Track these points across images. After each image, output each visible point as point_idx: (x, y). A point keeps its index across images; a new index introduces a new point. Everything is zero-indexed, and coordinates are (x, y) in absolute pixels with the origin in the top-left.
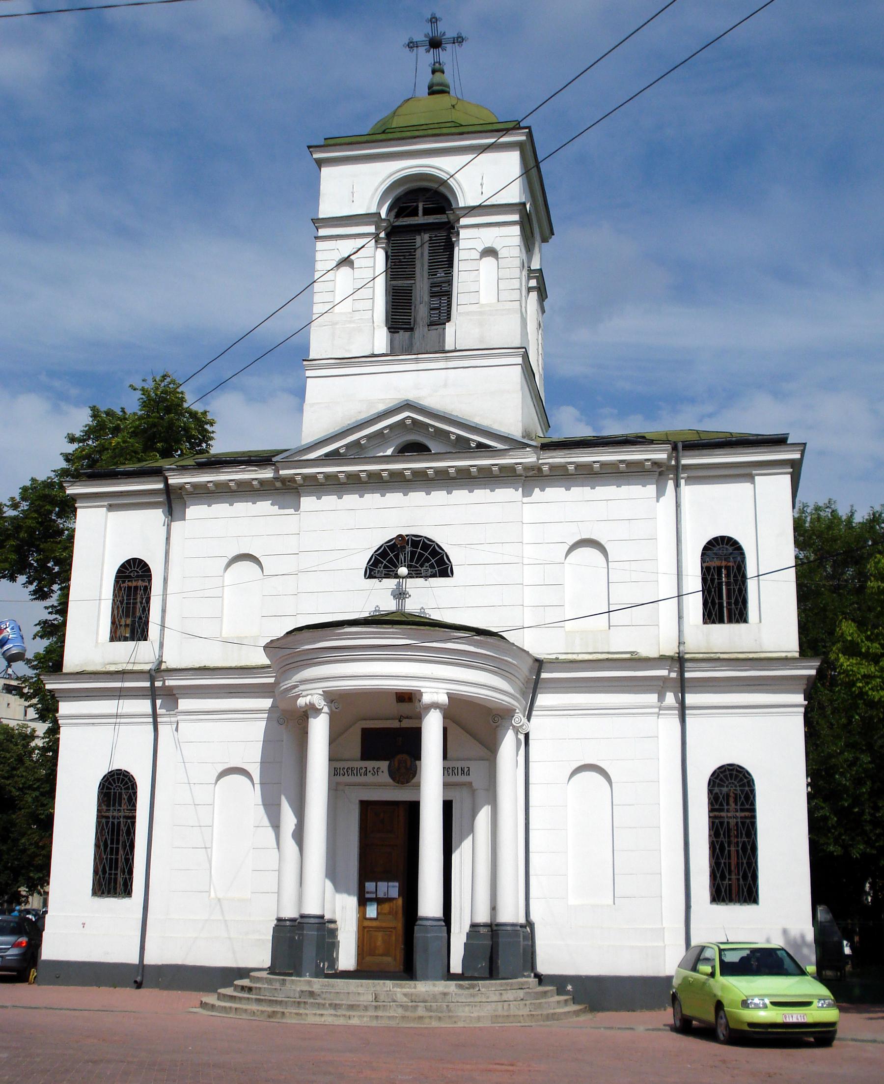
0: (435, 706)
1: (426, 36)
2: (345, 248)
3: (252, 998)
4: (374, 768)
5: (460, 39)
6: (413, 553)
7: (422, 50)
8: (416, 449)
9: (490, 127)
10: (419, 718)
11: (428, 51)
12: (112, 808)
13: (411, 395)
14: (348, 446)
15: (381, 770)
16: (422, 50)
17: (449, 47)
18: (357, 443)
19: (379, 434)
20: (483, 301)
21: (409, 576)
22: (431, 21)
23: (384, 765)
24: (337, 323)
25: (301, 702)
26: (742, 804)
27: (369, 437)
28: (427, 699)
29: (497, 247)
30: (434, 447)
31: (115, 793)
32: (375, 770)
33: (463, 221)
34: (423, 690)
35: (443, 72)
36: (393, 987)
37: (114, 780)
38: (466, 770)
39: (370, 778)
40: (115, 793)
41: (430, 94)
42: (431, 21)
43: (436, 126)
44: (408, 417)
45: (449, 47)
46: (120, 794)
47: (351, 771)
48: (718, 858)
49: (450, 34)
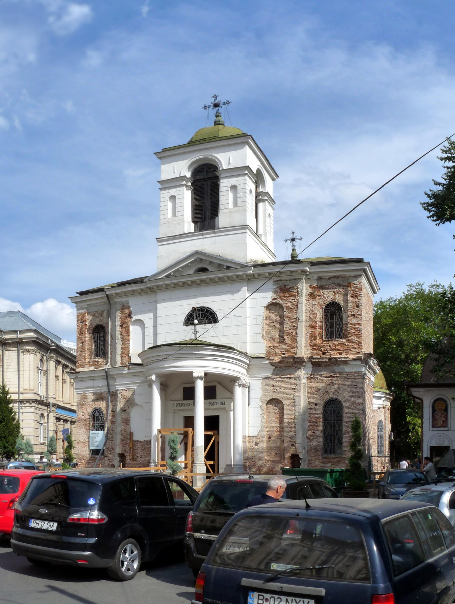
0: (201, 378)
1: (212, 103)
5: (228, 103)
6: (199, 314)
7: (210, 109)
8: (203, 270)
9: (234, 137)
10: (194, 383)
11: (213, 109)
12: (95, 423)
13: (200, 249)
14: (174, 272)
16: (210, 109)
17: (223, 106)
18: (178, 270)
19: (187, 265)
20: (230, 208)
21: (200, 324)
22: (214, 97)
24: (170, 222)
26: (337, 415)
27: (183, 267)
28: (195, 375)
29: (237, 185)
31: (96, 417)
34: (194, 371)
35: (221, 116)
37: (95, 412)
38: (223, 403)
39: (186, 407)
40: (96, 417)
41: (214, 125)
42: (214, 97)
43: (211, 138)
44: (198, 258)
45: (223, 106)
46: (98, 417)
47: (179, 405)
48: (326, 437)
49: (224, 100)
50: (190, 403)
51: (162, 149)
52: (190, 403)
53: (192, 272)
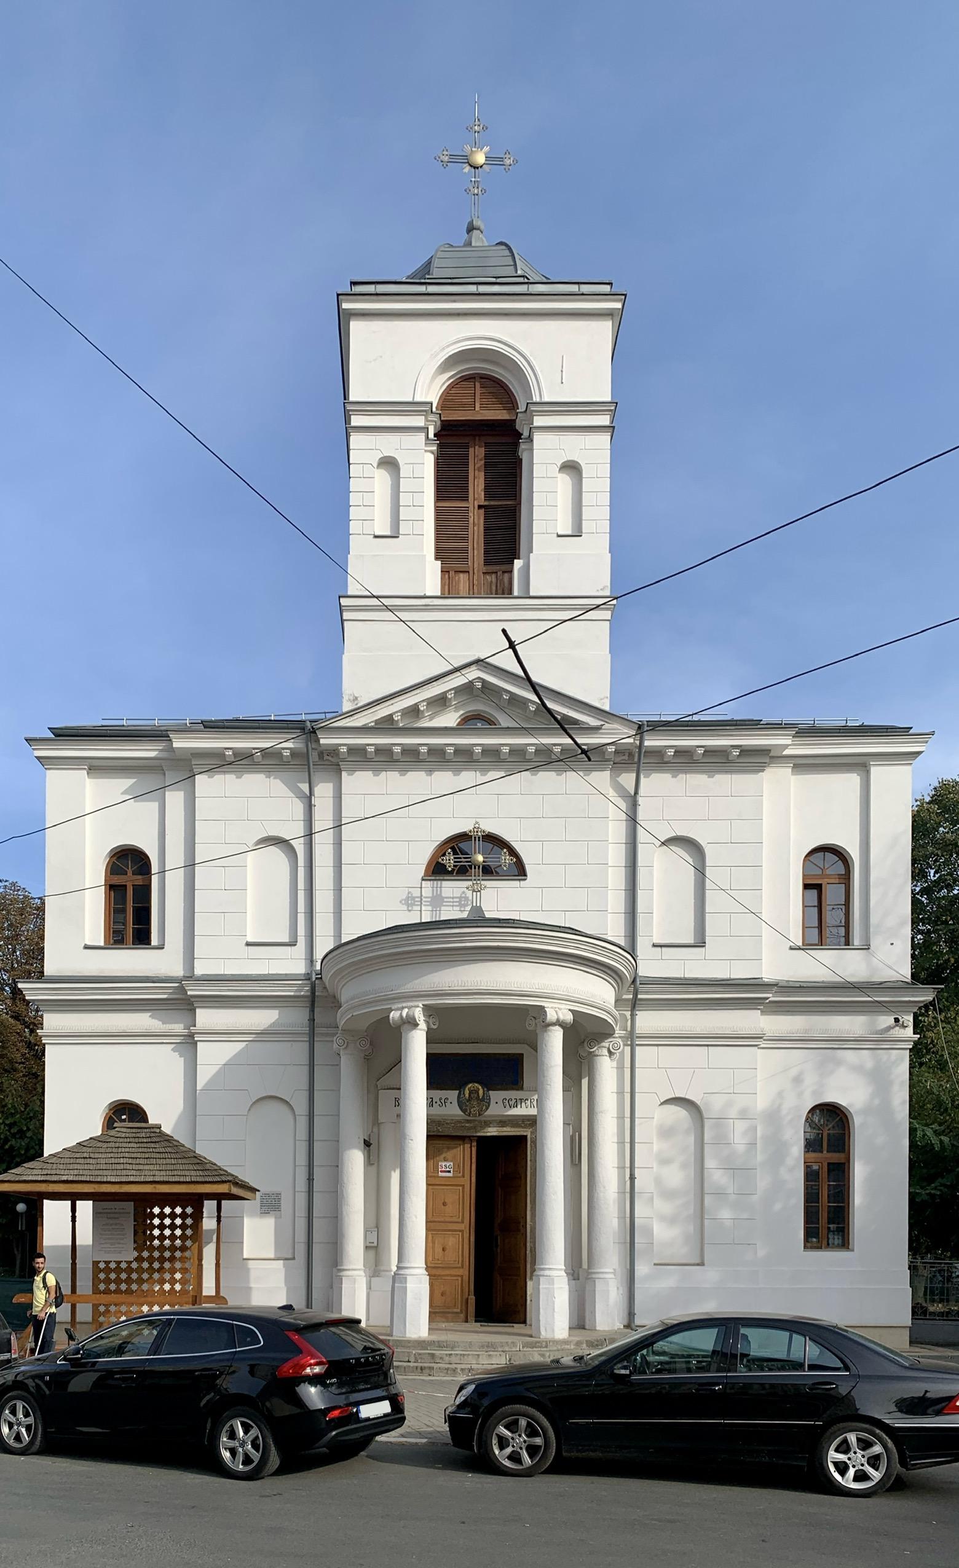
2: (389, 445)
3: (401, 1366)
4: (440, 1099)
15: (449, 1101)
23: (453, 1095)
25: (394, 1015)
28: (551, 1016)
30: (504, 721)
32: (443, 1101)
33: (538, 421)
36: (523, 1347)
50: (447, 1099)
51: (354, 283)
52: (447, 1099)
53: (450, 718)
